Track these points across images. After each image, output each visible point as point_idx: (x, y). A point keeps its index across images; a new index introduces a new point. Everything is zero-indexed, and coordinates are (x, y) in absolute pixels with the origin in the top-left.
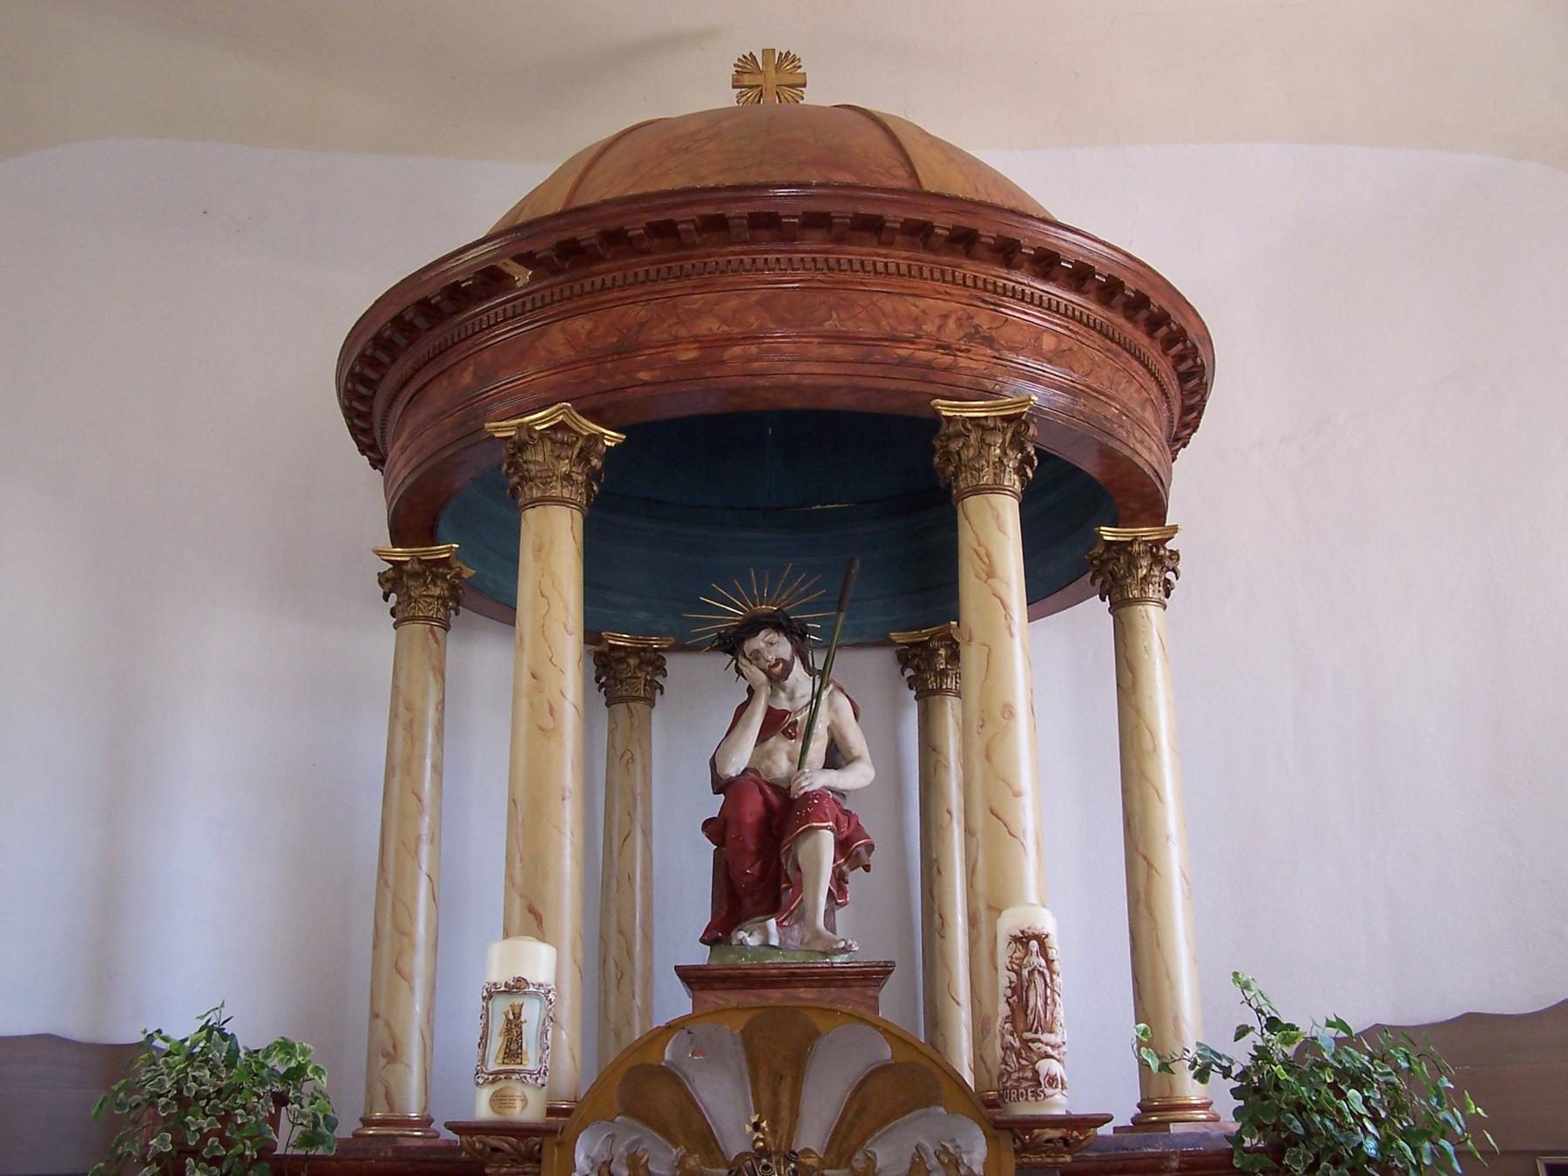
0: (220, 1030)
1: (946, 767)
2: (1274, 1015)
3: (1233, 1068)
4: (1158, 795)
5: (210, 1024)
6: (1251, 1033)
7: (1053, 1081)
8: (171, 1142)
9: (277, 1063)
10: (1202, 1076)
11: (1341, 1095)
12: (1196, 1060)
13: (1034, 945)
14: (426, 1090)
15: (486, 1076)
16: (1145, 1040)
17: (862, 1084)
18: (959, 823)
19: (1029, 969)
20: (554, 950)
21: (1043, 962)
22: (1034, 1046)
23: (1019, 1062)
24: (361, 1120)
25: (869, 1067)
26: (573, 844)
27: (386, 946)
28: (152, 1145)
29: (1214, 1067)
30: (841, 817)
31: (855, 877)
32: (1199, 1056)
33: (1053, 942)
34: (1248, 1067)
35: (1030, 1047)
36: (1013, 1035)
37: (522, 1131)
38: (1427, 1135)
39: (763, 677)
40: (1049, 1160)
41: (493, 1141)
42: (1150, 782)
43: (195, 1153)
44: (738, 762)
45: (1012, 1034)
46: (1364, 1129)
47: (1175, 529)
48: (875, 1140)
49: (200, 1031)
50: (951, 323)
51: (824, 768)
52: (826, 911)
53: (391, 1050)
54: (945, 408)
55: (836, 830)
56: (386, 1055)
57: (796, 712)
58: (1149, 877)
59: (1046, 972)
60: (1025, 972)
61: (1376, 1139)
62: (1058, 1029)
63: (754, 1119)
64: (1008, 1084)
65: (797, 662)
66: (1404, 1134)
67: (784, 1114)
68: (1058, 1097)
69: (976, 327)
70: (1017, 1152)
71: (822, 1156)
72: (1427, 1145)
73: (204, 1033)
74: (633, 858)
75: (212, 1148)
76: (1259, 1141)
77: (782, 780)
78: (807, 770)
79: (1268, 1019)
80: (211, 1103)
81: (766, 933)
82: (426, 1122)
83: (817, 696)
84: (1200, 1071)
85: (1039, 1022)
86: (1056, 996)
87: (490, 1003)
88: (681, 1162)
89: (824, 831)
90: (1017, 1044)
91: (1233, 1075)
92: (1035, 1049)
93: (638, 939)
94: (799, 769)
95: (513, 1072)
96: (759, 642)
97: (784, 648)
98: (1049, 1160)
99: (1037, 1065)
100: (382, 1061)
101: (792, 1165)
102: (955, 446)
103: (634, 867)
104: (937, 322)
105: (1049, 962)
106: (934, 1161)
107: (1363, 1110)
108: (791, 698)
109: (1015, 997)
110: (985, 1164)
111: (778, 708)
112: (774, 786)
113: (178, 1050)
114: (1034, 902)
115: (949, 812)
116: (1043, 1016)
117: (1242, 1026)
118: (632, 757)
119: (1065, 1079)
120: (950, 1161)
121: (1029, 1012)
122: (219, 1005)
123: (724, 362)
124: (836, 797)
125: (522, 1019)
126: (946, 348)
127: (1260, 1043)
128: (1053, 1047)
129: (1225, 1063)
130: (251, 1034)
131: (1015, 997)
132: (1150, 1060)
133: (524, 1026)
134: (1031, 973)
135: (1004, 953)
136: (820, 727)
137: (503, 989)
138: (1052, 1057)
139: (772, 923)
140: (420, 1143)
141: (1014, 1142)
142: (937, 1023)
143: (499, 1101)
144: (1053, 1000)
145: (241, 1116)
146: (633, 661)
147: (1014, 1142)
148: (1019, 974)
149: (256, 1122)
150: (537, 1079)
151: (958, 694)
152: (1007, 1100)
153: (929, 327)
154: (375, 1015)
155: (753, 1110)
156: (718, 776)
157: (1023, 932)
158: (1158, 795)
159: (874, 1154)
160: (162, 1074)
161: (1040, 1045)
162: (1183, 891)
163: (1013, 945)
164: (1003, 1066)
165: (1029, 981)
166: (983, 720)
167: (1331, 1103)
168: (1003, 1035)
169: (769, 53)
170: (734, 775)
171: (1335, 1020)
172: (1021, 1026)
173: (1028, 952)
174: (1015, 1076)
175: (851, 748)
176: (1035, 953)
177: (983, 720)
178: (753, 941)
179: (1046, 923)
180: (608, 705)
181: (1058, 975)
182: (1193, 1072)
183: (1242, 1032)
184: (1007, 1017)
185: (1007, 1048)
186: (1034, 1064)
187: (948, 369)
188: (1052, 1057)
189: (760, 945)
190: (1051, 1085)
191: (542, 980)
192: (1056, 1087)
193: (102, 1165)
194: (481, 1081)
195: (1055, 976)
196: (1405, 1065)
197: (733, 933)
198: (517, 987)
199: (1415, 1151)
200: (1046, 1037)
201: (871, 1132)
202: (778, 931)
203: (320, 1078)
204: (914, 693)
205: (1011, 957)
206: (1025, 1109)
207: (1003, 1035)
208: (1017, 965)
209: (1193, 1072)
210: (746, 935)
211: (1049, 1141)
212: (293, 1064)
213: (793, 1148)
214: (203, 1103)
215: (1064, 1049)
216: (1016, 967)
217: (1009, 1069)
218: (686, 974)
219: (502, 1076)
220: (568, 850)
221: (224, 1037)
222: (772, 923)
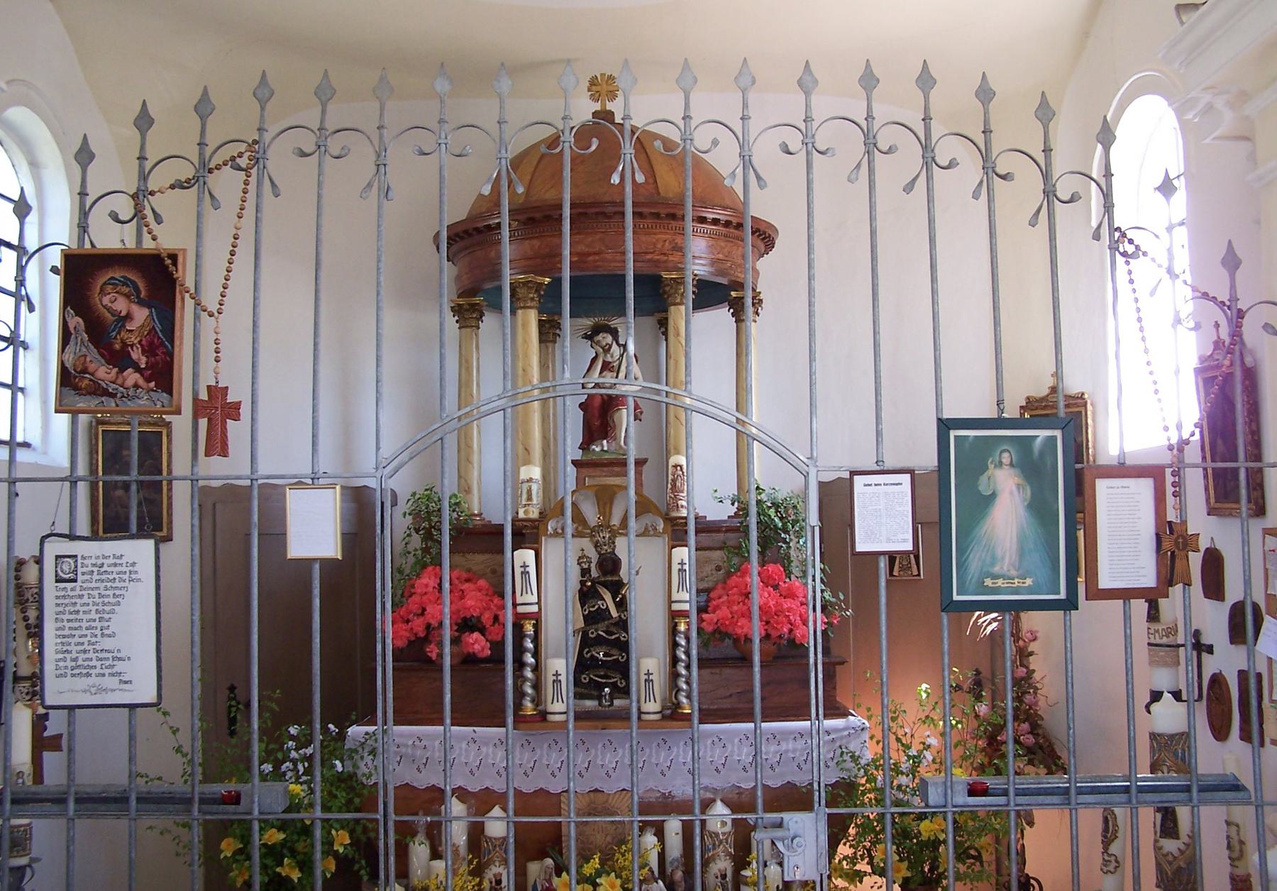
13: (679, 468)
14: (480, 503)
27: (463, 453)
39: (601, 350)
41: (525, 524)
43: (434, 527)
47: (760, 293)
50: (667, 244)
54: (665, 275)
56: (465, 491)
57: (615, 362)
65: (614, 343)
67: (607, 514)
69: (676, 243)
70: (672, 526)
74: (549, 407)
81: (603, 446)
82: (480, 515)
83: (622, 356)
88: (577, 528)
93: (552, 439)
96: (600, 337)
97: (609, 339)
102: (667, 289)
103: (549, 411)
104: (662, 244)
108: (612, 356)
123: (585, 262)
126: (664, 254)
139: (605, 442)
140: (480, 522)
143: (526, 512)
146: (547, 326)
153: (659, 246)
154: (460, 477)
169: (603, 75)
178: (598, 449)
187: (666, 262)
198: (530, 480)
200: (681, 494)
206: (674, 514)
218: (574, 462)
220: (536, 422)
222: (605, 442)
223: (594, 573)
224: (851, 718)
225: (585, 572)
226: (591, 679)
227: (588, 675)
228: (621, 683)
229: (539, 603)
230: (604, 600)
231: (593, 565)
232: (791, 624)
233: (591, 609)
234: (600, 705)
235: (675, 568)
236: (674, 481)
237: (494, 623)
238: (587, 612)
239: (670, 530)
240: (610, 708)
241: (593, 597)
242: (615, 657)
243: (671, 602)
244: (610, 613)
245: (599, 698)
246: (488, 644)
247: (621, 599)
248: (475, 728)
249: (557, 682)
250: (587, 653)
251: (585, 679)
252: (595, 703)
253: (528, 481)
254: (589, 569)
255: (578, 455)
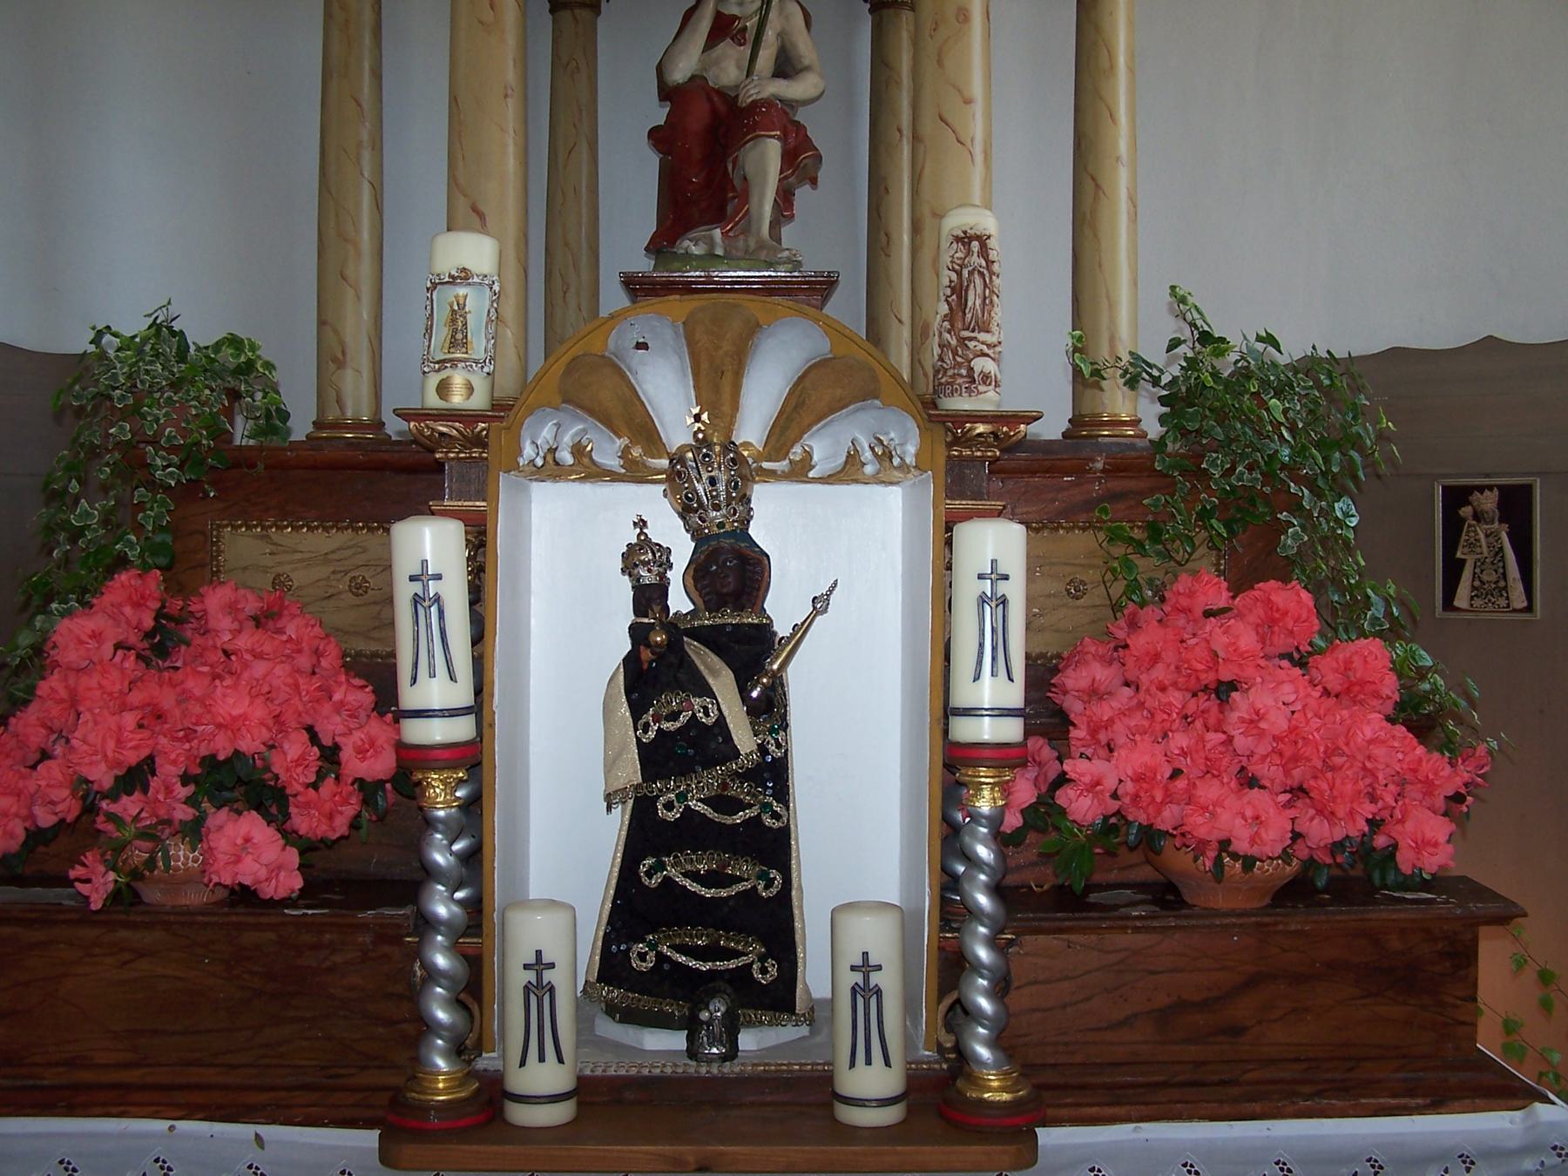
0: (170, 328)
1: (899, 83)
2: (1206, 328)
3: (1162, 377)
4: (1111, 115)
5: (158, 321)
6: (1183, 346)
7: (987, 378)
8: (130, 431)
9: (227, 356)
10: (1132, 383)
11: (1264, 405)
12: (1127, 369)
13: (975, 245)
15: (432, 365)
16: (1079, 345)
17: (801, 379)
18: (908, 143)
19: (970, 269)
20: (497, 242)
21: (984, 264)
22: (971, 344)
23: (954, 359)
24: (314, 423)
25: (808, 361)
26: (515, 144)
28: (111, 434)
29: (1144, 375)
30: (790, 127)
31: (803, 194)
32: (1131, 364)
33: (992, 243)
34: (1178, 377)
35: (966, 345)
36: (950, 333)
37: (467, 417)
38: (1338, 445)
40: (979, 454)
42: (1101, 98)
44: (680, 73)
45: (949, 332)
46: (1281, 436)
48: (812, 435)
49: (150, 327)
51: (773, 76)
52: (771, 222)
53: (340, 356)
55: (783, 139)
56: (335, 360)
57: (750, 18)
58: (1096, 198)
59: (985, 272)
60: (965, 273)
61: (1291, 447)
62: (994, 328)
63: (696, 410)
64: (943, 380)
66: (1317, 446)
68: (991, 394)
70: (949, 446)
71: (761, 449)
72: (1337, 455)
73: (153, 330)
75: (169, 438)
76: (1181, 447)
77: (730, 88)
78: (756, 78)
79: (1200, 333)
80: (166, 395)
81: (711, 243)
84: (1130, 379)
85: (977, 322)
86: (995, 298)
87: (435, 294)
89: (772, 140)
90: (954, 342)
91: (1162, 384)
92: (971, 347)
94: (747, 76)
95: (460, 360)
98: (979, 454)
99: (972, 363)
100: (332, 366)
101: (732, 455)
105: (989, 263)
106: (868, 455)
107: (1282, 419)
109: (954, 297)
110: (917, 455)
111: (726, 12)
112: (720, 93)
113: (128, 345)
114: (977, 202)
115: (900, 130)
116: (980, 316)
117: (1174, 339)
118: (578, 68)
119: (999, 377)
120: (884, 453)
121: (967, 311)
122: (165, 303)
124: (785, 107)
125: (467, 309)
127: (1190, 354)
128: (989, 346)
129: (1156, 373)
130: (200, 332)
131: (954, 297)
132: (1082, 366)
133: (468, 316)
134: (971, 273)
135: (950, 252)
136: (770, 33)
137: (447, 279)
138: (987, 355)
139: (717, 233)
141: (947, 435)
142: (879, 340)
144: (991, 301)
145: (195, 407)
147: (947, 435)
148: (959, 274)
149: (210, 414)
150: (482, 367)
151: (913, 9)
152: (942, 396)
155: (694, 401)
156: (665, 83)
157: (965, 232)
158: (1111, 115)
159: (811, 447)
160: (115, 368)
161: (977, 343)
162: (1128, 213)
163: (955, 245)
164: (940, 363)
165: (969, 281)
166: (936, 23)
167: (1252, 412)
168: (940, 334)
170: (681, 81)
171: (1264, 335)
172: (960, 325)
173: (969, 252)
174: (950, 373)
175: (801, 56)
176: (976, 254)
177: (936, 23)
179: (986, 222)
180: (552, 11)
181: (998, 276)
182: (1123, 380)
183: (1174, 344)
184: (946, 316)
185: (944, 346)
186: (970, 362)
188: (987, 355)
189: (706, 255)
190: (984, 383)
191: (485, 272)
192: (990, 384)
193: (65, 452)
194: (426, 369)
195: (994, 278)
196: (1327, 382)
197: (678, 242)
198: (463, 276)
199: (1326, 460)
200: (983, 336)
201: (809, 427)
202: (723, 242)
203: (270, 373)
204: (868, 6)
205: (953, 257)
207: (940, 334)
208: (959, 265)
209: (1123, 380)
210: (692, 244)
211: (980, 435)
212: (243, 359)
213: (733, 439)
214: (157, 395)
215: (998, 349)
216: (957, 267)
217: (945, 365)
219: (448, 365)
221: (173, 333)
222: (717, 233)
223: (679, 602)
224: (1539, 1107)
225: (649, 597)
226: (661, 958)
227: (653, 946)
228: (764, 971)
229: (479, 707)
230: (713, 696)
231: (676, 577)
232: (1357, 781)
233: (666, 726)
234: (693, 1052)
235: (967, 590)
236: (959, 291)
237: (321, 776)
238: (652, 734)
239: (941, 454)
240: (727, 1068)
241: (676, 686)
242: (740, 887)
243: (948, 712)
244: (728, 738)
245: (692, 1026)
246: (293, 856)
247: (765, 688)
248: (264, 1130)
249: (539, 991)
250: (649, 874)
251: (642, 957)
252: (676, 1041)
253: (453, 280)
254: (662, 588)
255: (643, 264)
